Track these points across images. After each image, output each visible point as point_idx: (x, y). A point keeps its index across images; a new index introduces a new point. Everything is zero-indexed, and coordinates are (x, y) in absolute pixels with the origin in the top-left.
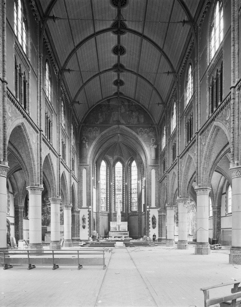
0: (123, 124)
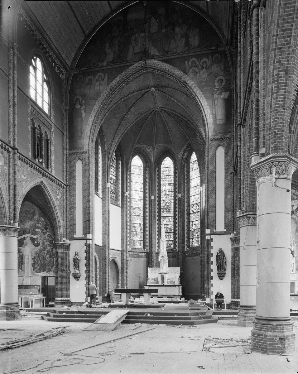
0: (154, 57)
